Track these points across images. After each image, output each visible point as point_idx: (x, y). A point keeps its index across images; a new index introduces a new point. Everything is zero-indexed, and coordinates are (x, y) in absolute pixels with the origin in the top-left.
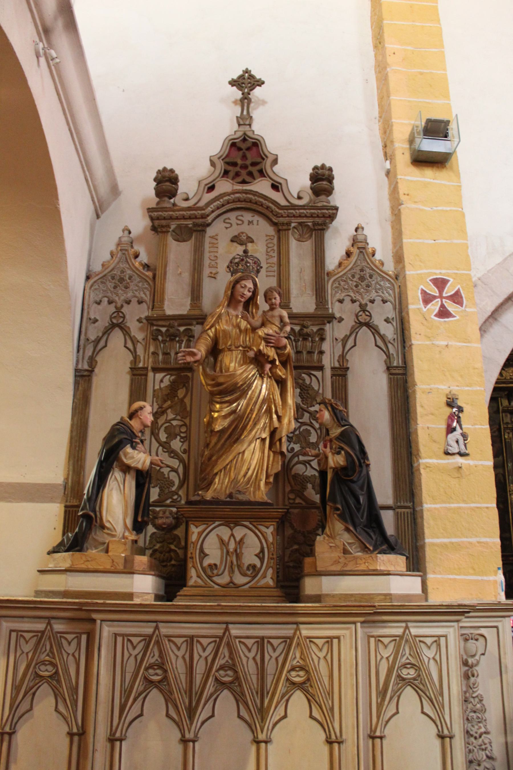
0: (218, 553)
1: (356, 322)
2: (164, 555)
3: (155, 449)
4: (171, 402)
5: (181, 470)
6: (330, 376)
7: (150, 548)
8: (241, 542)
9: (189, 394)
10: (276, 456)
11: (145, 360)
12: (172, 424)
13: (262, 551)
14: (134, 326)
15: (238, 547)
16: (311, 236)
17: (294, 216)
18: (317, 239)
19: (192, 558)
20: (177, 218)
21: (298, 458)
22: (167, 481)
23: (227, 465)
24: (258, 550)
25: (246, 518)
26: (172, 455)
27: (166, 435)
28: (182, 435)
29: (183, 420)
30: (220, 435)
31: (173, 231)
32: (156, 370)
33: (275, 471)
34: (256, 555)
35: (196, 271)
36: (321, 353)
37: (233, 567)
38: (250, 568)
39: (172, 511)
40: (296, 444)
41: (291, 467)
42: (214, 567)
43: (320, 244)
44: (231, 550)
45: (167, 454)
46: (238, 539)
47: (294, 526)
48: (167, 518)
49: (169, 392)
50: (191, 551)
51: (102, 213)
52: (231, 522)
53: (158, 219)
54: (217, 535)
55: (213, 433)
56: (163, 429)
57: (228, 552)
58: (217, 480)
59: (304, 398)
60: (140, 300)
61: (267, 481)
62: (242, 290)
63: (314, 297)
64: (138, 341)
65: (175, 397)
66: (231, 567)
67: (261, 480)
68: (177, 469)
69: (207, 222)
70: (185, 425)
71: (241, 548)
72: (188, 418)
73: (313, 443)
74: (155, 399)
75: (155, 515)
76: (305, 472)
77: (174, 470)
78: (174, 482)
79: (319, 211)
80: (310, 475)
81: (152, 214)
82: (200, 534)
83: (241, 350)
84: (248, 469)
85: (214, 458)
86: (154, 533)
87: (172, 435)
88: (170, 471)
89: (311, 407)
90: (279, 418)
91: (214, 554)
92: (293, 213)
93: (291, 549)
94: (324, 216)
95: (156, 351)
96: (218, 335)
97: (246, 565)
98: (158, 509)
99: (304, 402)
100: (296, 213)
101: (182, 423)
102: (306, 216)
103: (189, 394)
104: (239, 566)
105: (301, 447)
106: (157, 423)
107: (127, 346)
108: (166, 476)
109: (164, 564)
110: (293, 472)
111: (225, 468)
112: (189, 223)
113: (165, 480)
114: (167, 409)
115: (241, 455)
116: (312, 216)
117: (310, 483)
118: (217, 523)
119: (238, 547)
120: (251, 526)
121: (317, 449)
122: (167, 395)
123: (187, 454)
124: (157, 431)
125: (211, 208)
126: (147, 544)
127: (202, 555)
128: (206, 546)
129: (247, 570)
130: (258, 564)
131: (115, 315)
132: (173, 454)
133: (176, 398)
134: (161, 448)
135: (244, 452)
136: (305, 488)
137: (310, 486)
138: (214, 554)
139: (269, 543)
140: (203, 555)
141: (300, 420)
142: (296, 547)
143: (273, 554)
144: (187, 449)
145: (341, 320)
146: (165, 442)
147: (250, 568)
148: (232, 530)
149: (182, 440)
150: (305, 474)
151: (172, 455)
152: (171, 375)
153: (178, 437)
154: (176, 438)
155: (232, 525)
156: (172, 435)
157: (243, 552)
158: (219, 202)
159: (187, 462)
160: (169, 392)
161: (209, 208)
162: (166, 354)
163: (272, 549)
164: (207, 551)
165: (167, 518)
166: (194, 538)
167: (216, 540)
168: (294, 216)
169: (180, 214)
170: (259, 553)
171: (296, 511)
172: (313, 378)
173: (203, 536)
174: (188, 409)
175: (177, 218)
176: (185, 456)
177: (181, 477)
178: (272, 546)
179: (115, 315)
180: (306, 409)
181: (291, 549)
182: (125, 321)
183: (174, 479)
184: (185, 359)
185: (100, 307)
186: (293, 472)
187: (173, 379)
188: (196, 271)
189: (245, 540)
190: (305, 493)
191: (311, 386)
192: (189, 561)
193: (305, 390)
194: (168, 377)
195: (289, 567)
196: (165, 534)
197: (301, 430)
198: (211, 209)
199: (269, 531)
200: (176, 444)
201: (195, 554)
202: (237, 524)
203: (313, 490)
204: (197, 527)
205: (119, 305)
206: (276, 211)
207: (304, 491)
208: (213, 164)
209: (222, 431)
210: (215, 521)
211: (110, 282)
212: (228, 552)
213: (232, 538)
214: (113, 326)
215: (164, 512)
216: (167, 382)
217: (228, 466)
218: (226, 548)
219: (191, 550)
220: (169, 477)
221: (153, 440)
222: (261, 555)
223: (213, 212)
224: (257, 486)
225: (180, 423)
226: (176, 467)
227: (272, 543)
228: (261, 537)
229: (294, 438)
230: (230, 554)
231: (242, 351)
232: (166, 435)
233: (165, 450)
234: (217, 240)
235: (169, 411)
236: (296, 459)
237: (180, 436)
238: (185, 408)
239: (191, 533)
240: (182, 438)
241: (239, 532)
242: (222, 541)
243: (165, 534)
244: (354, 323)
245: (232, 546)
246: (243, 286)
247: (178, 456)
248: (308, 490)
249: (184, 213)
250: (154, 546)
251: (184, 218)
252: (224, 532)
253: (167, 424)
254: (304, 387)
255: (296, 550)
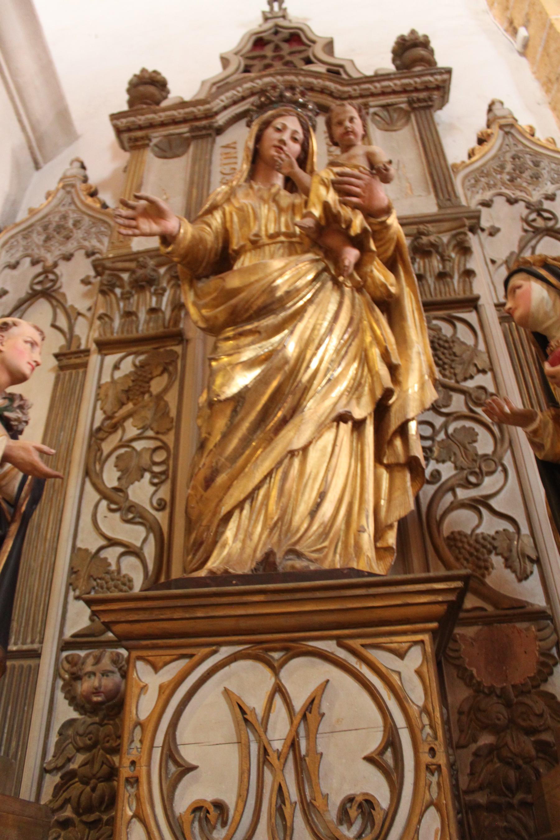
0: (231, 756)
1: (526, 231)
2: (93, 790)
3: (91, 508)
4: (135, 404)
5: (150, 551)
6: (497, 321)
7: (57, 769)
8: (309, 714)
9: (177, 384)
10: (398, 475)
11: (86, 333)
12: (133, 448)
13: (391, 741)
14: (75, 293)
15: (302, 732)
16: (408, 120)
17: (373, 95)
18: (420, 120)
19: (134, 781)
20: (163, 124)
21: (455, 495)
22: (113, 580)
23: (258, 488)
24: (375, 741)
25: (323, 628)
26: (130, 516)
27: (118, 474)
28: (156, 469)
29: (160, 436)
30: (235, 411)
31: (156, 145)
32: (105, 346)
33: (398, 513)
34: (369, 759)
35: (195, 186)
36: (469, 274)
37: (287, 810)
38: (353, 812)
39: (118, 654)
40: (443, 462)
41: (438, 518)
42: (213, 814)
43: (426, 126)
44: (278, 745)
45: (117, 515)
46: (298, 704)
47: (472, 676)
48: (105, 673)
49: (131, 384)
50: (133, 754)
51: (45, 162)
52: (273, 643)
53: (129, 130)
54: (227, 692)
55: (217, 406)
56: (112, 460)
57: (265, 752)
58: (229, 533)
59: (445, 363)
60: (90, 249)
61: (379, 545)
62: (277, 136)
63: (432, 196)
64: (79, 314)
65: (143, 393)
66: (280, 811)
67: (361, 530)
68: (141, 548)
69: (216, 125)
70: (164, 447)
71: (311, 737)
72: (172, 433)
73: (485, 455)
74: (99, 403)
75: (75, 669)
76: (478, 526)
77: (131, 551)
78: (130, 580)
79: (417, 80)
80: (492, 533)
81: (118, 123)
82: (167, 692)
83: (282, 242)
84: (322, 495)
85: (221, 479)
86: (70, 723)
87: (130, 472)
88: (123, 554)
89: (465, 379)
90: (393, 369)
91: (215, 766)
92: (369, 89)
93: (473, 747)
94: (427, 89)
95: (109, 313)
96: (228, 225)
97: (336, 801)
98: (82, 653)
99: (447, 373)
100: (376, 87)
101: (159, 444)
102: (394, 92)
103: (177, 384)
104: (309, 808)
105: (456, 468)
106: (100, 449)
107: (58, 324)
108: (114, 567)
109: (92, 817)
110: (446, 530)
111: (251, 496)
112: (184, 129)
113: (108, 577)
114: (125, 418)
115: (296, 462)
116: (405, 91)
117: (497, 554)
118: (225, 652)
119: (302, 732)
120: (342, 654)
121: (500, 468)
122: (127, 391)
123: (168, 510)
124: (98, 467)
125: (222, 101)
126: (49, 757)
127: (173, 768)
128: (184, 733)
129: (340, 822)
130: (383, 798)
131: (41, 278)
132: (132, 514)
133: (147, 396)
134: (104, 503)
135: (305, 449)
136: (487, 568)
137: (497, 561)
138: (215, 766)
139: (414, 711)
140: (179, 769)
141: (444, 410)
142: (486, 739)
143: (432, 751)
144: (168, 498)
145: (493, 232)
146: (116, 489)
147: (353, 812)
148: (276, 670)
149: (156, 481)
150: (479, 531)
151: (130, 516)
152: (137, 354)
153: (147, 476)
154: (142, 476)
155: (276, 655)
156: (130, 472)
157: (320, 749)
158: (235, 92)
159: (165, 529)
160: (131, 384)
161: (218, 101)
162: (128, 314)
163: (428, 730)
164: (188, 754)
165: (105, 673)
166: (144, 706)
167: (224, 714)
168: (373, 95)
169: (167, 116)
170: (382, 752)
171: (470, 631)
172: (459, 325)
173: (178, 702)
174: (173, 413)
175: (163, 124)
176: (162, 517)
177: (151, 566)
178: (426, 721)
179: (41, 278)
180: (456, 385)
181: (473, 747)
182: (58, 285)
183: (133, 575)
184: (136, 227)
185: (15, 272)
186: (446, 530)
187: (140, 362)
188: (195, 186)
189: (325, 707)
190: (488, 580)
191: (458, 339)
192: (126, 793)
193: (445, 348)
194: (130, 358)
195: (474, 808)
196: (101, 724)
197: (451, 430)
198: (222, 104)
199: (410, 666)
200: (142, 492)
201: (149, 765)
202: (293, 651)
203: (508, 571)
204: (156, 669)
205: (50, 262)
206: (339, 91)
207: (483, 576)
208: (225, 61)
209: (240, 399)
210: (220, 644)
211: (39, 234)
212: (265, 752)
213: (278, 699)
214: (33, 296)
215: (98, 660)
216: (127, 366)
217: (262, 492)
218: (259, 741)
219: (133, 749)
220: (119, 571)
221: (88, 486)
222: (389, 756)
223: (225, 108)
224: (351, 550)
225: (152, 444)
226: (138, 544)
227: (425, 710)
228: (381, 690)
229: (436, 449)
230: (273, 758)
231: (286, 244)
232: (118, 474)
233: (113, 506)
234: (235, 148)
235: (128, 423)
236: (449, 498)
237: (152, 472)
238: (166, 414)
239: (136, 691)
240: (155, 475)
241: (303, 677)
242: (243, 712)
243: (101, 724)
244: (523, 234)
245: (279, 730)
246: (279, 126)
247: (141, 517)
248: (494, 572)
249: (175, 113)
250: (69, 760)
251: (175, 122)
252: (250, 680)
253: (122, 451)
254: (441, 342)
255: (492, 749)
